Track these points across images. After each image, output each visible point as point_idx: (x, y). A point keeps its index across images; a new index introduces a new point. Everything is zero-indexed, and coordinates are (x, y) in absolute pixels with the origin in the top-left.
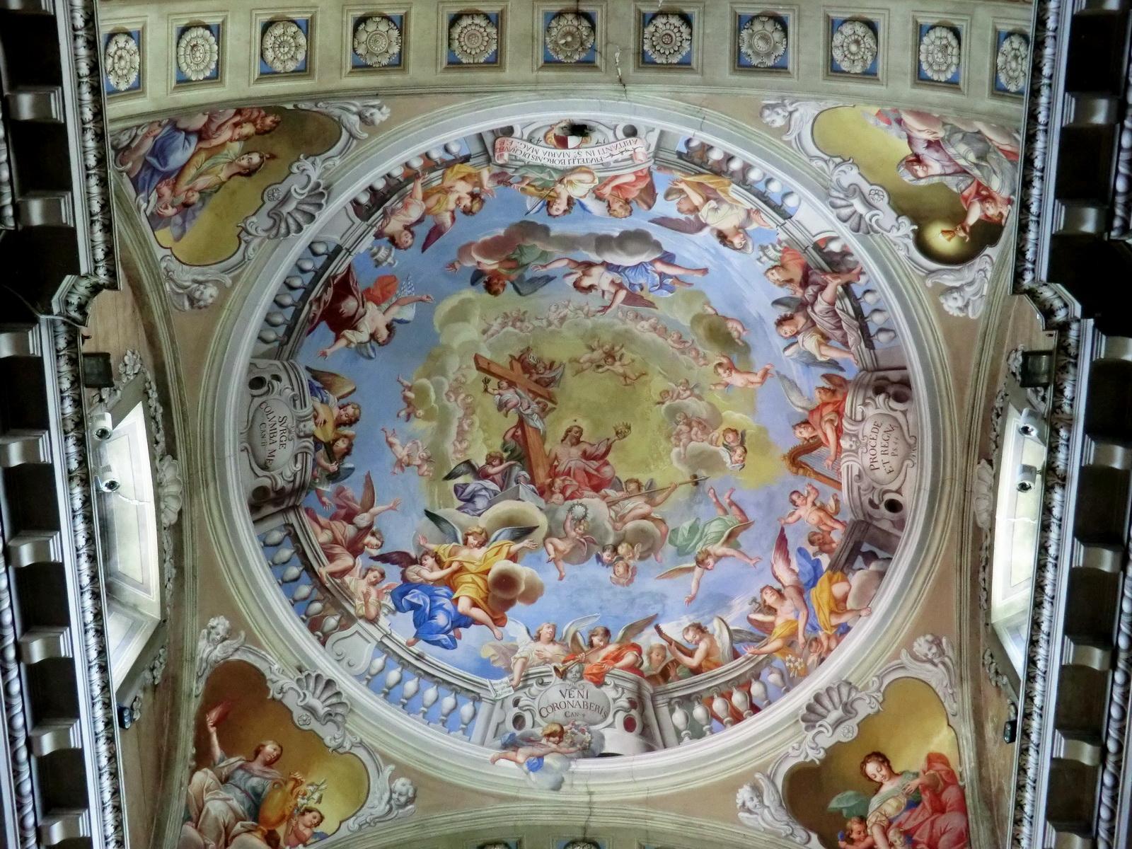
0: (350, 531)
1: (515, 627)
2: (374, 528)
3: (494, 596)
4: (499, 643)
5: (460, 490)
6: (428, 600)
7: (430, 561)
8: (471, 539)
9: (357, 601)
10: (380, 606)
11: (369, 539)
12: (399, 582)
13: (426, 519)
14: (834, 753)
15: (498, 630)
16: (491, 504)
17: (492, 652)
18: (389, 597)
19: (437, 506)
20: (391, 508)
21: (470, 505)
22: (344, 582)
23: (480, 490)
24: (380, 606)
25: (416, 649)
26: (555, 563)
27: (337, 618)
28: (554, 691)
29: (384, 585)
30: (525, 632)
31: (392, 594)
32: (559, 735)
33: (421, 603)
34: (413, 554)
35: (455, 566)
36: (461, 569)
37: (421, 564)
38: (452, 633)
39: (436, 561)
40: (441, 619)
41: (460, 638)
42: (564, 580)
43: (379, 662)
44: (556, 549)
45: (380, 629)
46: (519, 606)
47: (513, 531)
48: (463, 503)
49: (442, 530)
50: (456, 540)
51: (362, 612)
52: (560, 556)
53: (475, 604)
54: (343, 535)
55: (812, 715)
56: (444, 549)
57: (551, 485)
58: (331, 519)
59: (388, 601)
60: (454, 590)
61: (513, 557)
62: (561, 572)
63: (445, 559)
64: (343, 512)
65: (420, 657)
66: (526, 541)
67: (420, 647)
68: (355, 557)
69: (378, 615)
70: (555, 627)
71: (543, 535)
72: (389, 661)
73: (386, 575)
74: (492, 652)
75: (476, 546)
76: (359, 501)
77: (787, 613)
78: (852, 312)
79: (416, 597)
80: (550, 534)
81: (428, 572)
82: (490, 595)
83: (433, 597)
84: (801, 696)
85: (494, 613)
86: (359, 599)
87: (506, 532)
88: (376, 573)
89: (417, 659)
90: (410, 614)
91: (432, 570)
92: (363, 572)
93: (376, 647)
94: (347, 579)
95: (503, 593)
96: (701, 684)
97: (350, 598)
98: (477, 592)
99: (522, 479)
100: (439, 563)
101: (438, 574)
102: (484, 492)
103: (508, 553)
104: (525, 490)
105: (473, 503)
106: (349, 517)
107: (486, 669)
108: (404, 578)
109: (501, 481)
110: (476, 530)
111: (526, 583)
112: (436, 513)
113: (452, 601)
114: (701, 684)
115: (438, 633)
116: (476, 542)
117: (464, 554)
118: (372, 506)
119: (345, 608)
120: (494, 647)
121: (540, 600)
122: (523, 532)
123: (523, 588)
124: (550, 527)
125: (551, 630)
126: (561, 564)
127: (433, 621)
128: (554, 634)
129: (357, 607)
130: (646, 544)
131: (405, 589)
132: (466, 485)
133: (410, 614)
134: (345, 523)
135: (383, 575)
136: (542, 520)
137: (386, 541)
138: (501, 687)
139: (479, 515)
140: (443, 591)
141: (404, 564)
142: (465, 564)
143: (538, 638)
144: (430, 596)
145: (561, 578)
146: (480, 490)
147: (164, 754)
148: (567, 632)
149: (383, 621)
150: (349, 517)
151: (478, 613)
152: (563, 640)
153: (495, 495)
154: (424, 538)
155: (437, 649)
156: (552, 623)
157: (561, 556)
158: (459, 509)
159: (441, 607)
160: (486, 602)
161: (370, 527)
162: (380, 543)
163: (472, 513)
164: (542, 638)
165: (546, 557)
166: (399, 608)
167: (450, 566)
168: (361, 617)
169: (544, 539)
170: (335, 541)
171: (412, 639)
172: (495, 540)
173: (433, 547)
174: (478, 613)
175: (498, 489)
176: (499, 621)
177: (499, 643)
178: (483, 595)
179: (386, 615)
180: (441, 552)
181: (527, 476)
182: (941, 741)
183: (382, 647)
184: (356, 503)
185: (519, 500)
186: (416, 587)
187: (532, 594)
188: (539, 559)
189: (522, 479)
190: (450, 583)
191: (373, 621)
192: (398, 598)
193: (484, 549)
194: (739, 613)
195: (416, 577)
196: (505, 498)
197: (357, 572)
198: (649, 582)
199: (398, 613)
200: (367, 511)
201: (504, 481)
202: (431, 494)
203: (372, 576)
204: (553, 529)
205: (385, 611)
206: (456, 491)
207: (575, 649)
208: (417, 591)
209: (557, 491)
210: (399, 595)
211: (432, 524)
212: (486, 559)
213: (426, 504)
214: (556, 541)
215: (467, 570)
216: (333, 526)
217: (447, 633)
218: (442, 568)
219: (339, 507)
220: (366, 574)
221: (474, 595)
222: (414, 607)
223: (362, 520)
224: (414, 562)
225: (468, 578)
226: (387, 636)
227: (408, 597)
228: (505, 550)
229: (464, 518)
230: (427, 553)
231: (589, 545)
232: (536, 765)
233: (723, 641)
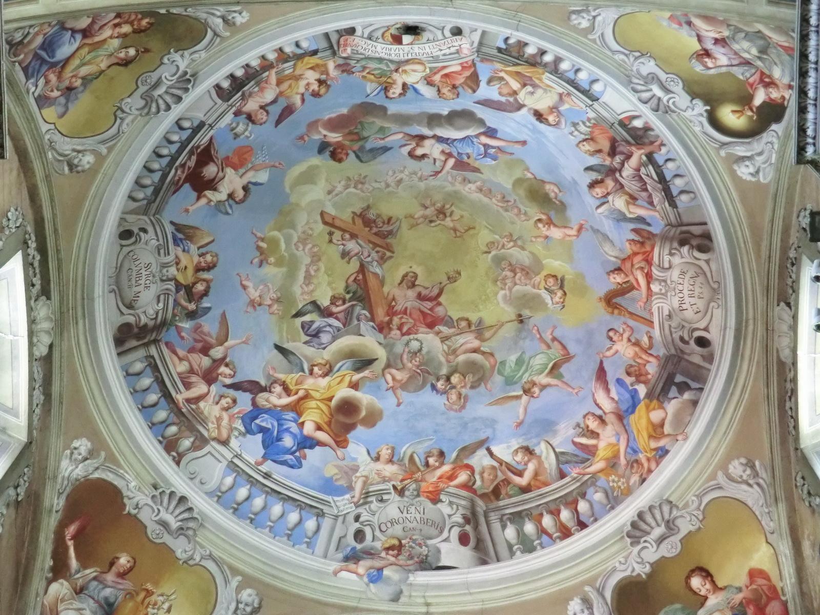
1: (357, 449)
14: (659, 566)
28: (393, 508)
32: (398, 548)
55: (636, 531)
77: (608, 438)
84: (626, 513)
95: (345, 418)
96: (531, 502)
107: (329, 487)
114: (531, 502)
122: (364, 363)
130: (477, 374)
138: (343, 504)
176: (341, 443)
182: (761, 558)
187: (372, 419)
190: (297, 408)
194: (564, 436)
198: (480, 407)
207: (412, 469)
231: (425, 375)
232: (376, 577)
233: (550, 462)
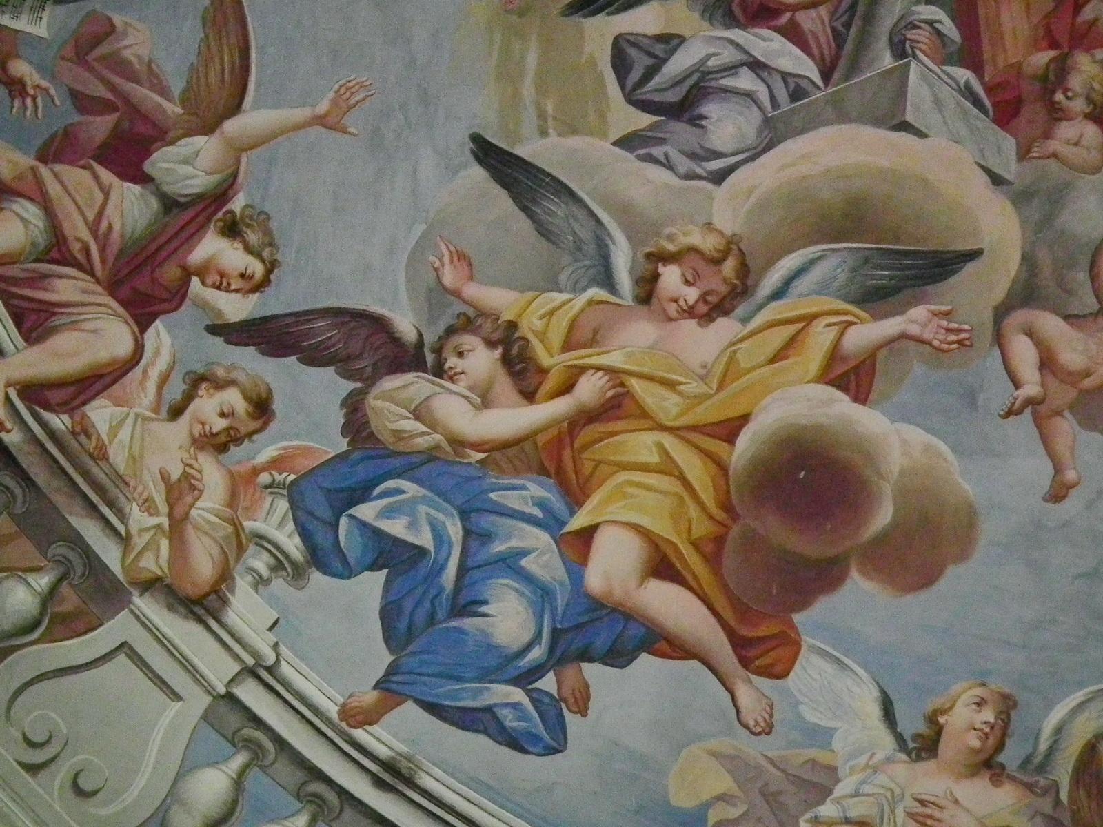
0: (130, 208)
1: (832, 691)
2: (238, 204)
3: (752, 541)
4: (753, 748)
5: (641, 63)
6: (454, 530)
7: (479, 360)
8: (671, 277)
9: (136, 515)
10: (240, 541)
11: (212, 247)
12: (332, 443)
13: (477, 174)
15: (752, 692)
16: (773, 134)
17: (722, 782)
18: (283, 505)
19: (529, 121)
20: (320, 120)
21: (680, 130)
22: (84, 429)
23: (731, 69)
24: (240, 541)
25: (381, 739)
26: (1038, 421)
27: (43, 581)
29: (265, 450)
30: (874, 711)
31: (294, 492)
33: (425, 539)
34: (406, 326)
35: (589, 389)
36: (617, 407)
37: (439, 371)
38: (548, 683)
39: (507, 361)
40: (508, 619)
41: (582, 704)
42: (1072, 505)
43: (211, 786)
44: (1047, 363)
45: (231, 641)
46: (860, 600)
47: (866, 260)
48: (645, 120)
49: (544, 231)
50: (607, 280)
51: (155, 562)
52: (1062, 395)
53: (662, 566)
54: (94, 229)
56: (545, 315)
57: (1059, 74)
58: (44, 156)
59: (275, 522)
60: (575, 496)
61: (853, 377)
62: (1058, 469)
63: (549, 357)
64: (100, 127)
65: (394, 775)
66: (919, 312)
67: (400, 732)
68: (143, 322)
69: (225, 577)
70: (1007, 705)
71: (1000, 292)
72: (257, 782)
73: (277, 406)
74: (722, 782)
75: (690, 312)
76: (177, 86)
78: (707, 497)
79: (406, 513)
80: (1026, 293)
81: (470, 407)
82: (735, 530)
83: (475, 515)
85: (744, 612)
86: (149, 506)
87: (832, 263)
88: (233, 398)
89: (379, 783)
90: (371, 586)
91: (485, 399)
92: (176, 390)
93: (207, 717)
94: (100, 413)
95: (793, 529)
97: (103, 498)
98: (677, 516)
99: (922, 36)
100: (522, 370)
101: (512, 418)
102: (745, 81)
103: (835, 354)
104: (931, 87)
105: (696, 121)
106: (128, 153)
108: (356, 422)
109: (825, 38)
110: (696, 238)
111: (902, 495)
112: (521, 151)
113: (560, 541)
115: (487, 675)
116: (692, 294)
117: (634, 341)
118: (235, 108)
119: (77, 542)
120: (732, 762)
121: (955, 578)
122: (912, 266)
123: (883, 516)
124: (1028, 260)
125: (988, 715)
126: (1066, 426)
127: (468, 623)
128: (1001, 733)
129: (132, 541)
131: (362, 472)
132: (670, 42)
133: (371, 586)
134: (106, 175)
135: (262, 408)
136: (998, 228)
137: (287, 256)
139: (719, 178)
140: (531, 492)
141: (365, 363)
142: (636, 385)
143: (926, 746)
144: (464, 515)
145: (1058, 493)
146: (731, 69)
147: (14, 289)
148: (1059, 730)
149: (247, 610)
150: (128, 153)
151: (670, 604)
152: (1037, 766)
153: (797, 94)
154: (462, 257)
155: (477, 746)
156: (996, 684)
157: (1069, 394)
158: (627, 142)
159: (510, 564)
160: (714, 559)
161: (220, 195)
162: (258, 269)
163: (684, 164)
164: (947, 747)
165: (998, 393)
166: (322, 557)
167: (566, 388)
168: (150, 585)
169: (1001, 312)
170: (57, 249)
171: (370, 697)
172: (778, 295)
173: (499, 299)
174: (670, 604)
175: (809, 69)
176: (762, 648)
177: (753, 748)
178: (702, 528)
179: (260, 582)
180: (531, 324)
181: (949, 27)
183: (234, 720)
184: (164, 92)
185: (904, 127)
186: (406, 472)
187: (923, 547)
188: (970, 397)
189: (922, 36)
190: (561, 460)
191: (204, 606)
192: (324, 511)
193: (725, 328)
195: (410, 425)
196: (843, 117)
197: (143, 389)
199: (317, 578)
200: (208, 129)
201: (839, 38)
202: (508, 74)
203: (209, 408)
204: (1046, 269)
205: (260, 562)
206: (621, 64)
208: (411, 489)
209: (1079, 105)
210: (327, 498)
211: (502, 202)
212: (730, 371)
213: (480, 110)
214: (1050, 324)
215: (644, 414)
216: (54, 189)
217: (525, 679)
218: (529, 396)
219: (83, 102)
220: (189, 397)
221: (663, 528)
222: (390, 555)
223: (187, 164)
224: (406, 358)
225: (641, 445)
226: (260, 672)
227: (366, 511)
228: (821, 338)
229: (644, 184)
230: (465, 325)
